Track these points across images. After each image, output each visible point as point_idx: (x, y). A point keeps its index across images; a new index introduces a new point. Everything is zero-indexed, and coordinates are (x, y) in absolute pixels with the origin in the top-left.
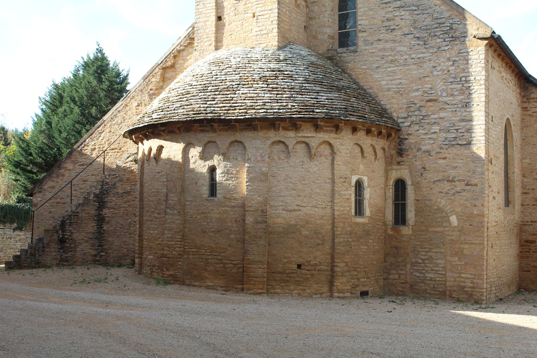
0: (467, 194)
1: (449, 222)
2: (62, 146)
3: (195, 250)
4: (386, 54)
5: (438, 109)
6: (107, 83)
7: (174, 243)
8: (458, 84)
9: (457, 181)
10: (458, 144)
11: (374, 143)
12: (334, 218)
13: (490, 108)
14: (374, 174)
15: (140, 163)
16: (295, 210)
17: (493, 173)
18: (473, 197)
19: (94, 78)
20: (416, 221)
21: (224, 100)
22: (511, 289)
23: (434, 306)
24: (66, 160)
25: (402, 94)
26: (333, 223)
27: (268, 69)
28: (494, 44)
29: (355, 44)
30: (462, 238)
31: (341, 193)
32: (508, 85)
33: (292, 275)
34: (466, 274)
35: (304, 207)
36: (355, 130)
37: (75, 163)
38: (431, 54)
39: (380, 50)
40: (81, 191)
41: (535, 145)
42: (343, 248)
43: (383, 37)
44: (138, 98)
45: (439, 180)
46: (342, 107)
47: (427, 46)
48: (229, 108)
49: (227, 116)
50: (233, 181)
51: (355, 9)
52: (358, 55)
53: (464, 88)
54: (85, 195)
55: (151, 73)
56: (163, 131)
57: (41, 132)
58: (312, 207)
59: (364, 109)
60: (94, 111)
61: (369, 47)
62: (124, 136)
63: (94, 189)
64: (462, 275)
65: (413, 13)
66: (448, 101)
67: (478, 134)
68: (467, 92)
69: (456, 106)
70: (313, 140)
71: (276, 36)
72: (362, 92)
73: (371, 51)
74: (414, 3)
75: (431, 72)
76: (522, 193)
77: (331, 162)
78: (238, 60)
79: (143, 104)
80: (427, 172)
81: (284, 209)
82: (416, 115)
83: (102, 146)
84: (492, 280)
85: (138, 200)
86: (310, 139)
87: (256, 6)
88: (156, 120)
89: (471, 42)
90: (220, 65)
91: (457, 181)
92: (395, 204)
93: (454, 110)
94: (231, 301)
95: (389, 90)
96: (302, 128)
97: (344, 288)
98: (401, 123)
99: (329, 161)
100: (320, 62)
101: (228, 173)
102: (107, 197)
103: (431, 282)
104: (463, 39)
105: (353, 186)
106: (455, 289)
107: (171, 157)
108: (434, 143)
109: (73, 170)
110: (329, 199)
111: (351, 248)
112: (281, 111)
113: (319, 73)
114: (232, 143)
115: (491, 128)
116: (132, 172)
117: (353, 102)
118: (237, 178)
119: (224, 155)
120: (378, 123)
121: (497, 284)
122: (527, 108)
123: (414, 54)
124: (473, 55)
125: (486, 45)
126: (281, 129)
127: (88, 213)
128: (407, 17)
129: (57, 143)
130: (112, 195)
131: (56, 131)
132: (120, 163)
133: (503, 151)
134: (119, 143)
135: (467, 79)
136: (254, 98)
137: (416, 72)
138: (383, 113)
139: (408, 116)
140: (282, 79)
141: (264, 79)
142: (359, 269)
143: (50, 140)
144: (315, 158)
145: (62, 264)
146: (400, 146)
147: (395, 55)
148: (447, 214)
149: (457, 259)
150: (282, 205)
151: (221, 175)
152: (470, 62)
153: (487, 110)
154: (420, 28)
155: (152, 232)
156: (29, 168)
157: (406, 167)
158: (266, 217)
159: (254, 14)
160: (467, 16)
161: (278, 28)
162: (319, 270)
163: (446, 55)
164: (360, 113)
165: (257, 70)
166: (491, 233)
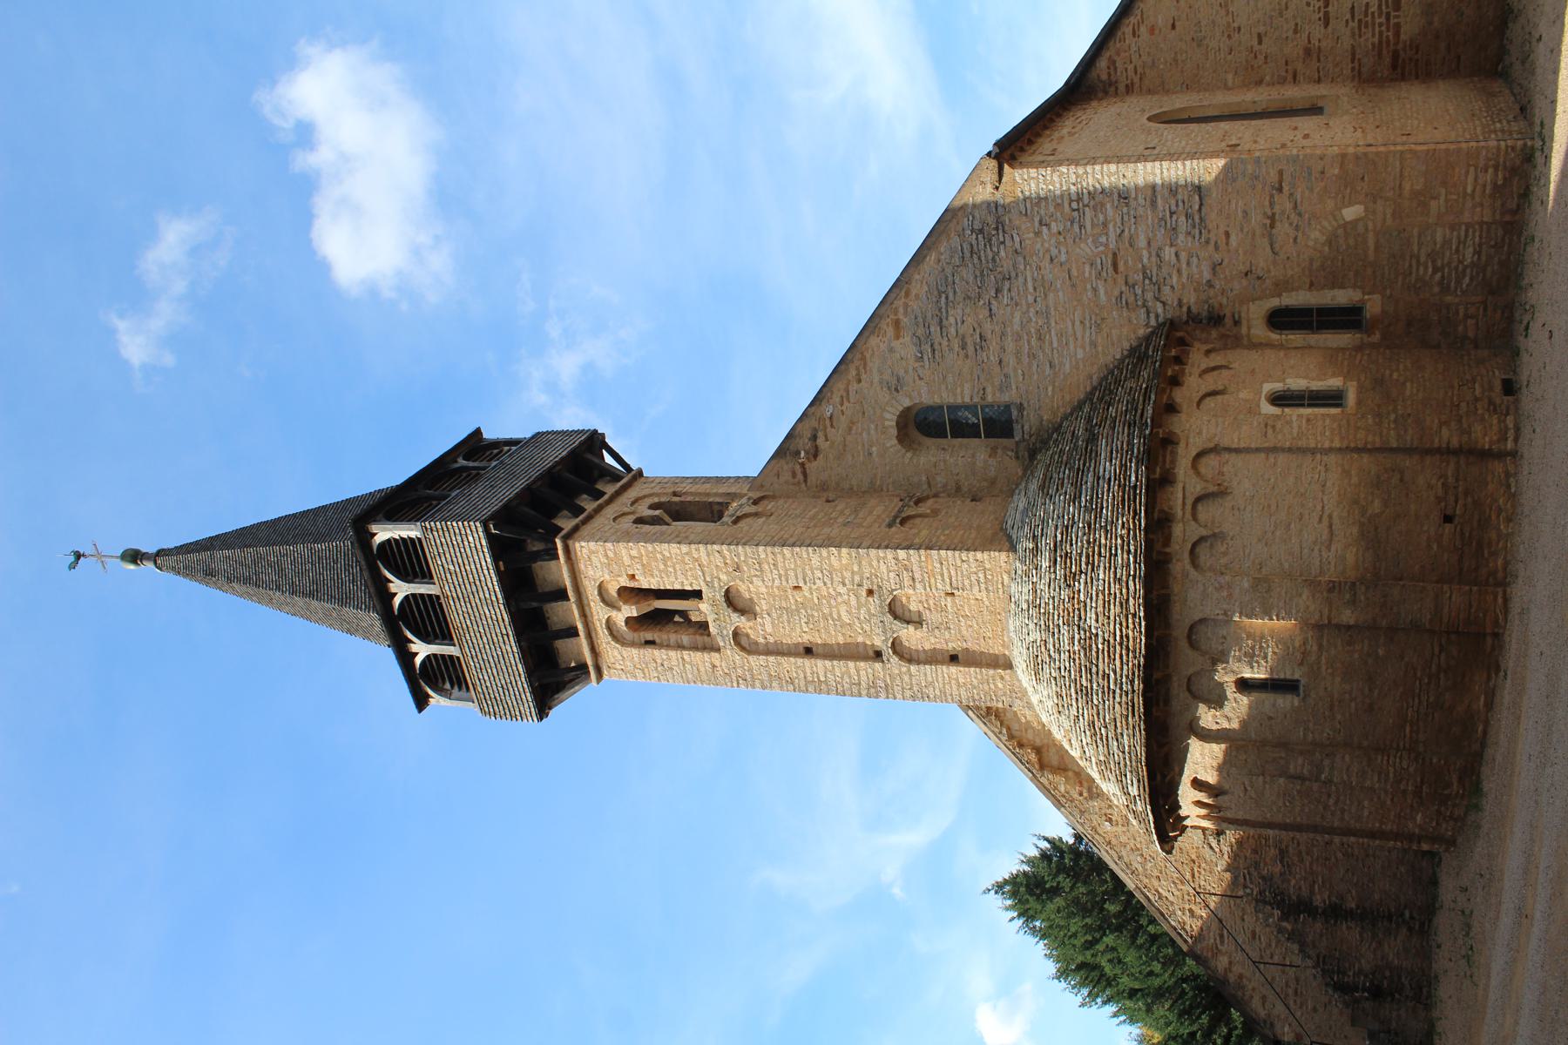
0: (1300, 190)
1: (1356, 221)
2: (1179, 973)
5: (1131, 250)
6: (1060, 878)
9: (1272, 209)
10: (1200, 209)
11: (1196, 371)
12: (1348, 449)
13: (1130, 153)
14: (1257, 370)
15: (1224, 825)
16: (1330, 526)
17: (1255, 142)
18: (1304, 178)
20: (1354, 287)
21: (1109, 656)
22: (1498, 90)
23: (1537, 244)
24: (1209, 968)
25: (1103, 319)
26: (1358, 450)
27: (1052, 571)
28: (1009, 152)
29: (1008, 407)
30: (1390, 194)
31: (1295, 435)
32: (1084, 122)
33: (1467, 534)
34: (1466, 184)
35: (1323, 507)
36: (1171, 408)
37: (1216, 952)
38: (1028, 267)
39: (1019, 361)
40: (1274, 945)
41: (1198, 65)
42: (1410, 431)
44: (1096, 819)
47: (1013, 275)
48: (1124, 647)
49: (1140, 653)
51: (943, 407)
52: (1028, 402)
53: (1092, 203)
54: (1283, 939)
56: (1164, 776)
57: (1149, 1010)
58: (1323, 492)
59: (1130, 391)
60: (1112, 908)
61: (1012, 381)
62: (1169, 852)
63: (1271, 920)
64: (1469, 190)
65: (952, 302)
66: (1115, 231)
67: (1180, 173)
68: (1099, 198)
69: (1126, 218)
70: (1189, 489)
71: (990, 555)
72: (1097, 394)
73: (1021, 379)
75: (1061, 265)
76: (1294, 83)
77: (1234, 455)
78: (1032, 626)
79: (1109, 811)
80: (1254, 268)
81: (1326, 547)
82: (1143, 292)
83: (1186, 897)
84: (1479, 129)
85: (1298, 835)
86: (1187, 494)
87: (934, 591)
89: (1006, 194)
90: (1040, 662)
91: (1272, 209)
92: (1318, 329)
93: (1133, 220)
94: (1522, 660)
95: (1094, 344)
96: (1166, 509)
97: (1495, 428)
98: (1157, 320)
99: (1233, 457)
100: (1040, 473)
101: (1252, 656)
102: (1290, 898)
103: (1484, 253)
104: (999, 208)
105: (1283, 411)
106: (1499, 203)
107: (1215, 764)
108: (1198, 256)
109: (1230, 957)
110: (1309, 457)
111: (1409, 415)
112: (1132, 548)
114: (1193, 644)
115: (1168, 150)
116: (1240, 843)
118: (1262, 637)
119: (1214, 662)
120: (1158, 364)
121: (1489, 118)
122: (1127, 86)
123: (1027, 297)
124: (1030, 190)
125: (1011, 166)
127: (1321, 936)
128: (960, 311)
129: (1171, 983)
131: (1149, 983)
132: (1221, 865)
133: (1212, 124)
135: (1074, 197)
136: (1106, 599)
137: (1060, 294)
138: (1138, 355)
140: (1071, 545)
141: (1070, 579)
142: (1455, 399)
143: (1165, 996)
144: (1225, 484)
145: (1427, 999)
146: (1201, 320)
148: (1339, 226)
149: (1433, 204)
151: (1256, 670)
152: (1042, 194)
153: (1133, 159)
154: (979, 288)
155: (1366, 813)
157: (1244, 308)
158: (1343, 584)
159: (947, 594)
160: (958, 203)
162: (1457, 480)
164: (1139, 397)
165: (1052, 591)
166: (1379, 138)
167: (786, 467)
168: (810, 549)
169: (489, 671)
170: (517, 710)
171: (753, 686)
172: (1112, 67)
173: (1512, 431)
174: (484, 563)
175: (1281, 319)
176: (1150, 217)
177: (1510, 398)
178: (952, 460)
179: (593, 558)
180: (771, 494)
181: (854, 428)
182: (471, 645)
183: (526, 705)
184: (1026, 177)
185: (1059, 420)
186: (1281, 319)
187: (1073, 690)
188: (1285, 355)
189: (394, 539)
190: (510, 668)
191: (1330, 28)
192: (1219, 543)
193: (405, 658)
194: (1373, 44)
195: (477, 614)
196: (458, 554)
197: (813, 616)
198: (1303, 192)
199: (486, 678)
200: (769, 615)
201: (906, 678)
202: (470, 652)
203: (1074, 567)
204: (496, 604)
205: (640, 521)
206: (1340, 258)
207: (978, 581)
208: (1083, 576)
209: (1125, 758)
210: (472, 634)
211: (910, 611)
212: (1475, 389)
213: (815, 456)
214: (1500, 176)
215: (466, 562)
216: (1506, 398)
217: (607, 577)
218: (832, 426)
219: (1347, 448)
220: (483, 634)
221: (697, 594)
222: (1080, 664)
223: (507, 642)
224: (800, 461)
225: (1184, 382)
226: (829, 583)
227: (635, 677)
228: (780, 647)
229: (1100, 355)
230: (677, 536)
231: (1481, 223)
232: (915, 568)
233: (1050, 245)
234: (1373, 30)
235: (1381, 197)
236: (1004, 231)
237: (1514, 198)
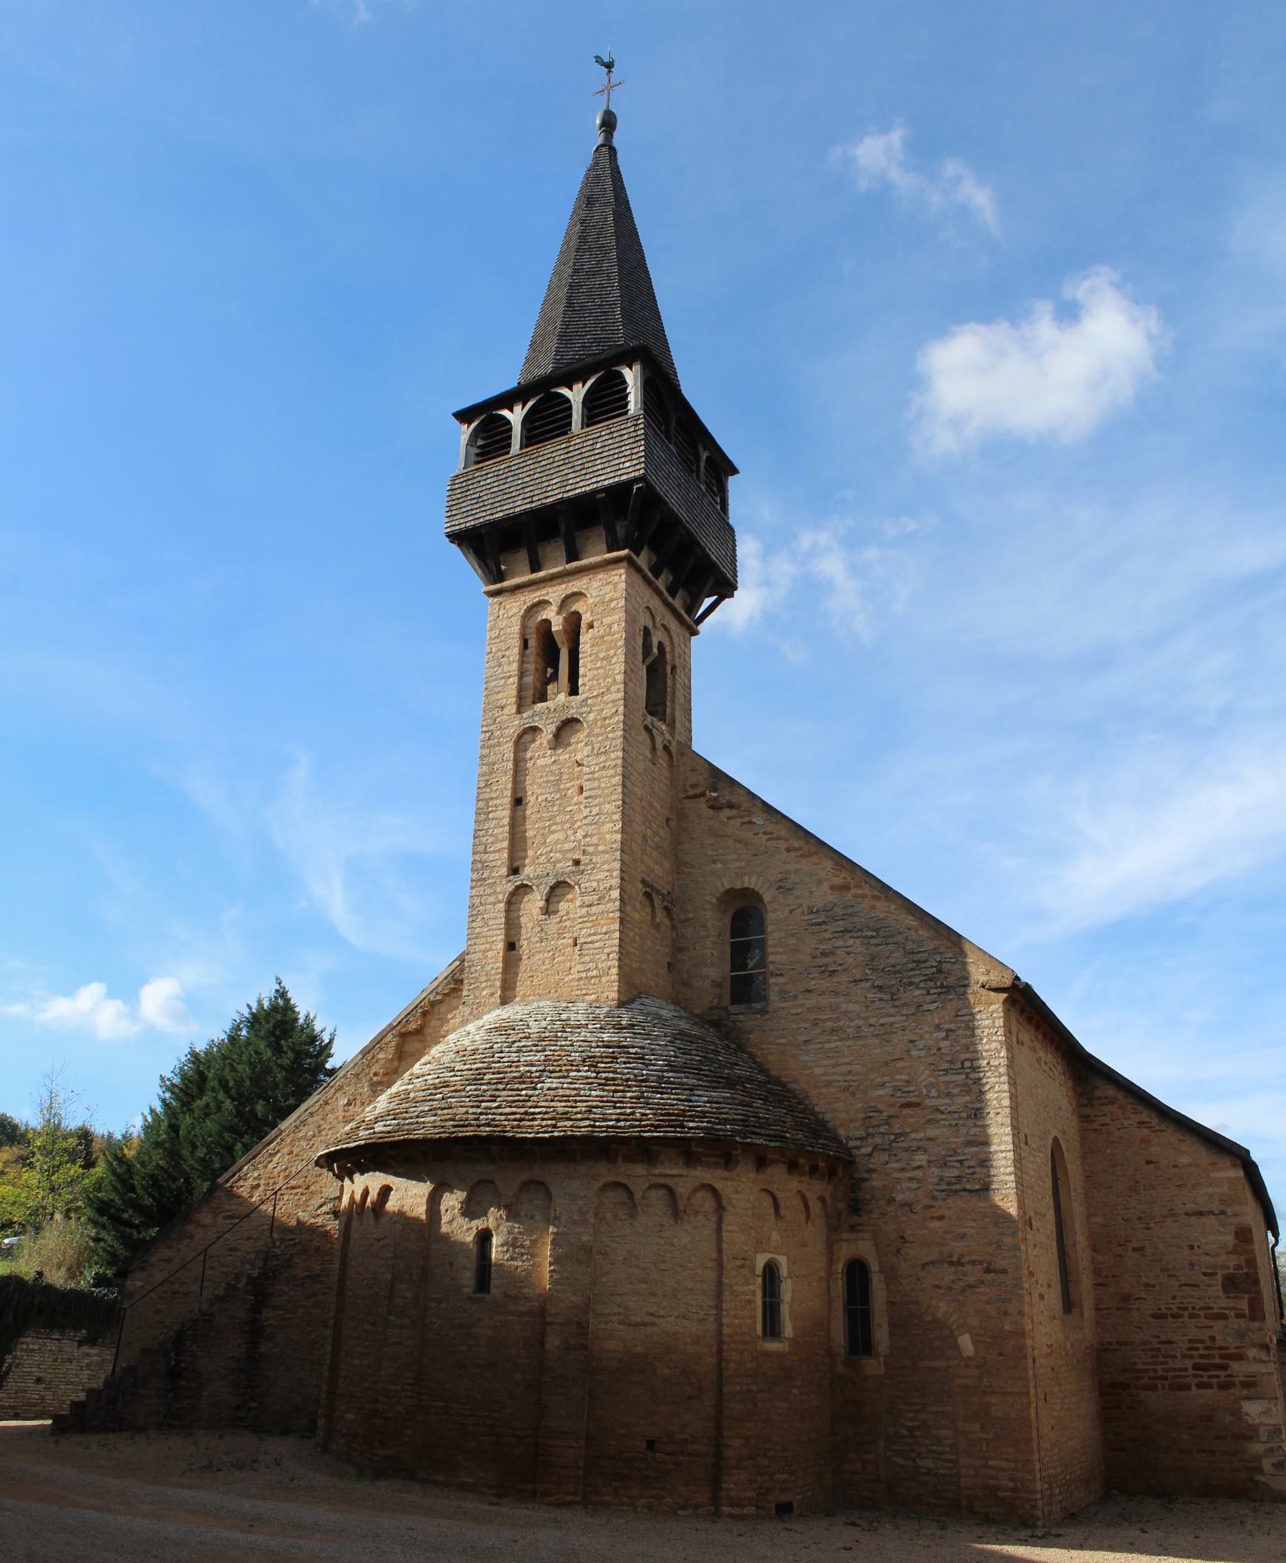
0: (988, 1290)
2: (194, 1175)
3: (440, 1404)
4: (821, 1017)
5: (924, 1121)
7: (399, 1387)
8: (958, 1074)
9: (968, 1263)
10: (965, 1190)
12: (721, 1343)
13: (1020, 1119)
15: (344, 1219)
17: (1035, 1246)
19: (267, 1046)
21: (514, 1101)
23: (939, 1533)
25: (854, 1093)
26: (720, 1352)
27: (599, 1044)
29: (765, 998)
31: (735, 1288)
32: (1051, 1074)
35: (663, 1317)
38: (904, 1018)
39: (810, 1010)
40: (222, 1270)
41: (1111, 1187)
43: (815, 985)
45: (932, 1263)
46: (738, 1117)
47: (897, 1003)
48: (523, 1116)
49: (517, 1132)
50: (523, 1261)
51: (763, 934)
52: (769, 1019)
53: (970, 1082)
55: (377, 1043)
57: (157, 1145)
58: (678, 1317)
62: (317, 1163)
64: (992, 1463)
66: (942, 1105)
68: (975, 1089)
69: (956, 1116)
72: (779, 1088)
73: (794, 1012)
74: (871, 925)
75: (907, 1051)
76: (1095, 1284)
78: (544, 1024)
79: (358, 1102)
80: (908, 1245)
82: (882, 1133)
83: (272, 1181)
84: (1052, 1471)
86: (676, 1179)
88: (381, 1135)
90: (508, 1032)
91: (968, 1263)
93: (953, 1123)
95: (829, 1084)
96: (661, 1157)
98: (854, 1148)
99: (712, 1225)
101: (514, 1245)
105: (758, 1276)
107: (405, 1209)
108: (919, 1188)
111: (755, 1405)
112: (622, 1124)
113: (694, 1052)
114: (525, 1186)
115: (1025, 1158)
116: (326, 1234)
117: (758, 1108)
118: (533, 1256)
119: (508, 1208)
120: (810, 1149)
121: (1064, 1481)
124: (982, 1020)
125: (1005, 1001)
126: (620, 1160)
128: (859, 950)
131: (185, 1145)
133: (1052, 1202)
134: (306, 1177)
136: (571, 1098)
137: (878, 1051)
138: (819, 1128)
139: (868, 1135)
140: (625, 1063)
143: (172, 1160)
144: (686, 1218)
147: (838, 1019)
149: (977, 1426)
150: (619, 1314)
151: (499, 1249)
152: (978, 1032)
153: (1015, 1123)
154: (883, 969)
155: (356, 1362)
156: (126, 1216)
159: (575, 940)
160: (967, 948)
161: (619, 967)
163: (932, 1019)
165: (579, 1044)
167: (701, 778)
168: (620, 803)
169: (496, 484)
170: (457, 512)
171: (482, 747)
172: (1106, 1101)
173: (740, 1513)
174: (603, 478)
175: (857, 1273)
176: (957, 1140)
177: (773, 1511)
178: (708, 943)
179: (610, 587)
180: (675, 763)
181: (741, 846)
182: (521, 465)
183: (462, 521)
184: (995, 1015)
185: (749, 1050)
186: (857, 1273)
187: (480, 1065)
188: (822, 1278)
189: (626, 388)
190: (498, 504)
191: (1149, 1319)
192: (626, 1212)
193: (508, 400)
194: (1135, 1363)
195: (552, 471)
196: (612, 452)
197: (553, 805)
199: (489, 481)
200: (554, 762)
201: (492, 899)
202: (515, 465)
203: (603, 1065)
204: (563, 490)
205: (647, 633)
206: (920, 1332)
207: (588, 970)
208: (594, 1075)
209: (411, 1118)
210: (532, 467)
211: (559, 902)
212: (783, 1473)
213: (712, 807)
215: (604, 460)
217: (591, 601)
218: (743, 823)
219: (722, 1341)
220: (532, 478)
221: (574, 691)
222: (506, 1072)
223: (525, 501)
224: (707, 792)
226: (587, 821)
227: (491, 629)
228: (522, 773)
229: (817, 1091)
230: (632, 670)
232: (601, 907)
233: (927, 1039)
234: (1150, 1364)
236: (939, 994)
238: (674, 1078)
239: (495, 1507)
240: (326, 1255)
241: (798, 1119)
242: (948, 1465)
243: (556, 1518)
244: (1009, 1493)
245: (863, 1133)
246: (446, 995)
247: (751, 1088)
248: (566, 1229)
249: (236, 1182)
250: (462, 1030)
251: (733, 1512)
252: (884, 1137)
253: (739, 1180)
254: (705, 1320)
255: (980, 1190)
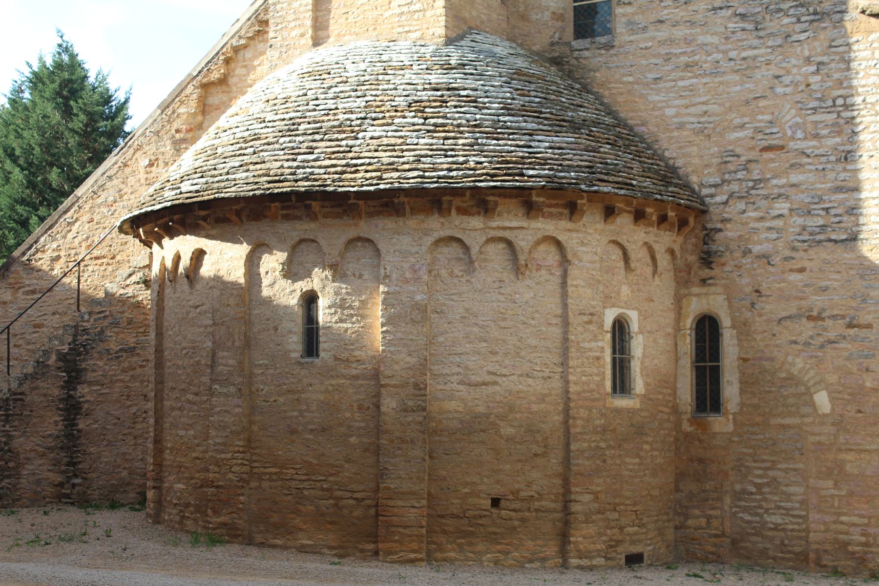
0: (849, 346)
1: (813, 405)
4: (674, 51)
5: (787, 165)
7: (229, 456)
8: (829, 112)
9: (829, 317)
10: (830, 240)
11: (650, 239)
15: (156, 287)
18: (862, 351)
20: (742, 404)
21: (334, 153)
25: (709, 136)
26: (567, 410)
29: (609, 31)
30: (841, 439)
31: (582, 345)
33: (480, 522)
35: (505, 376)
38: (769, 50)
39: (662, 43)
43: (668, 14)
45: (789, 317)
46: (583, 163)
47: (762, 33)
49: (339, 186)
50: (354, 323)
52: (615, 55)
53: (842, 121)
55: (177, 96)
56: (204, 219)
58: (521, 376)
62: (121, 229)
64: (844, 518)
66: (808, 148)
68: (847, 129)
69: (823, 159)
75: (771, 88)
77: (560, 281)
78: (363, 66)
79: (161, 162)
80: (763, 299)
82: (739, 179)
83: (73, 252)
86: (515, 232)
90: (323, 77)
91: (829, 317)
93: (820, 167)
95: (681, 126)
96: (499, 209)
97: (592, 547)
98: (707, 196)
99: (556, 280)
101: (342, 307)
102: (85, 360)
105: (607, 332)
106: (828, 547)
107: (221, 273)
108: (778, 238)
110: (557, 360)
111: (605, 461)
112: (454, 173)
113: (533, 93)
114: (351, 242)
116: (138, 305)
117: (605, 153)
118: (363, 317)
119: (334, 267)
120: (659, 197)
124: (859, 51)
126: (454, 212)
130: (95, 355)
134: (111, 246)
136: (396, 148)
137: (738, 88)
139: (723, 181)
140: (455, 107)
141: (417, 107)
144: (527, 272)
148: (808, 388)
149: (830, 483)
150: (458, 374)
151: (327, 311)
152: (854, 65)
155: (182, 433)
158: (424, 398)
162: (537, 510)
163: (802, 51)
165: (402, 87)
173: (589, 564)
176: (823, 186)
177: (623, 561)
198: (847, 349)
206: (774, 389)
208: (422, 121)
209: (221, 175)
214: (857, 548)
216: (623, 557)
225: (639, 226)
231: (807, 531)
235: (838, 431)
237: (833, 561)
238: (511, 122)
239: (337, 567)
240: (141, 327)
241: (645, 165)
242: (797, 520)
243: (400, 574)
244: (860, 548)
245: (718, 180)
246: (249, 38)
247: (598, 132)
248: (397, 288)
249: (34, 255)
250: (271, 76)
251: (583, 564)
252: (741, 184)
253: (586, 232)
254: (550, 378)
255: (846, 240)
